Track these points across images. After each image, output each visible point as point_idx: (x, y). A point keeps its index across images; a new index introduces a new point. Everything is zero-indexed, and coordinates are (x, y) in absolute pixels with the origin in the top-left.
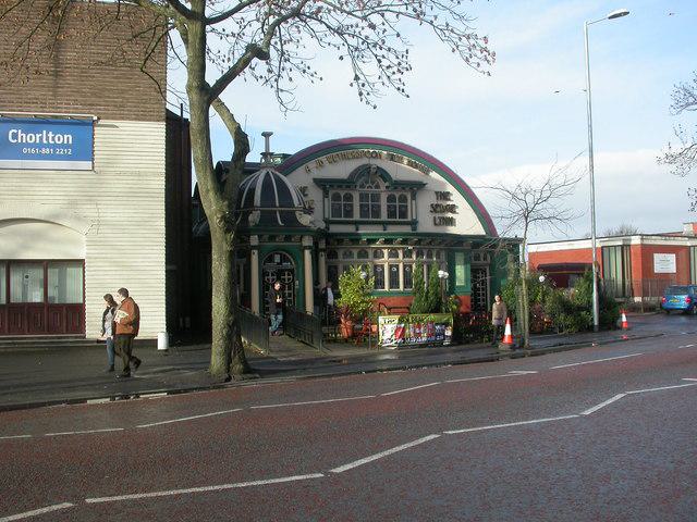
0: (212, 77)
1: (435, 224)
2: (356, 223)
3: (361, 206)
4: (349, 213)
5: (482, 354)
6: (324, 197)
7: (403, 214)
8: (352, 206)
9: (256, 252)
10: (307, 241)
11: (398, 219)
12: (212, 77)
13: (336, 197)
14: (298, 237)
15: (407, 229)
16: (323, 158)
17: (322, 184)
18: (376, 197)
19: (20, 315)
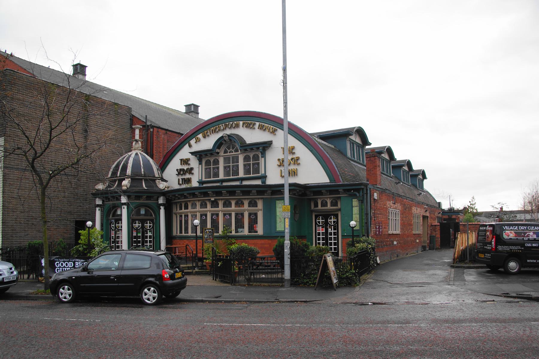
0: (45, 182)
1: (179, 184)
2: (222, 181)
3: (245, 165)
4: (236, 172)
5: (263, 298)
6: (200, 164)
7: (257, 171)
8: (238, 166)
9: (126, 207)
10: (161, 201)
11: (231, 177)
12: (45, 182)
13: (208, 163)
14: (155, 197)
15: (258, 182)
16: (200, 136)
17: (200, 155)
18: (236, 160)
19: (4, 73)
